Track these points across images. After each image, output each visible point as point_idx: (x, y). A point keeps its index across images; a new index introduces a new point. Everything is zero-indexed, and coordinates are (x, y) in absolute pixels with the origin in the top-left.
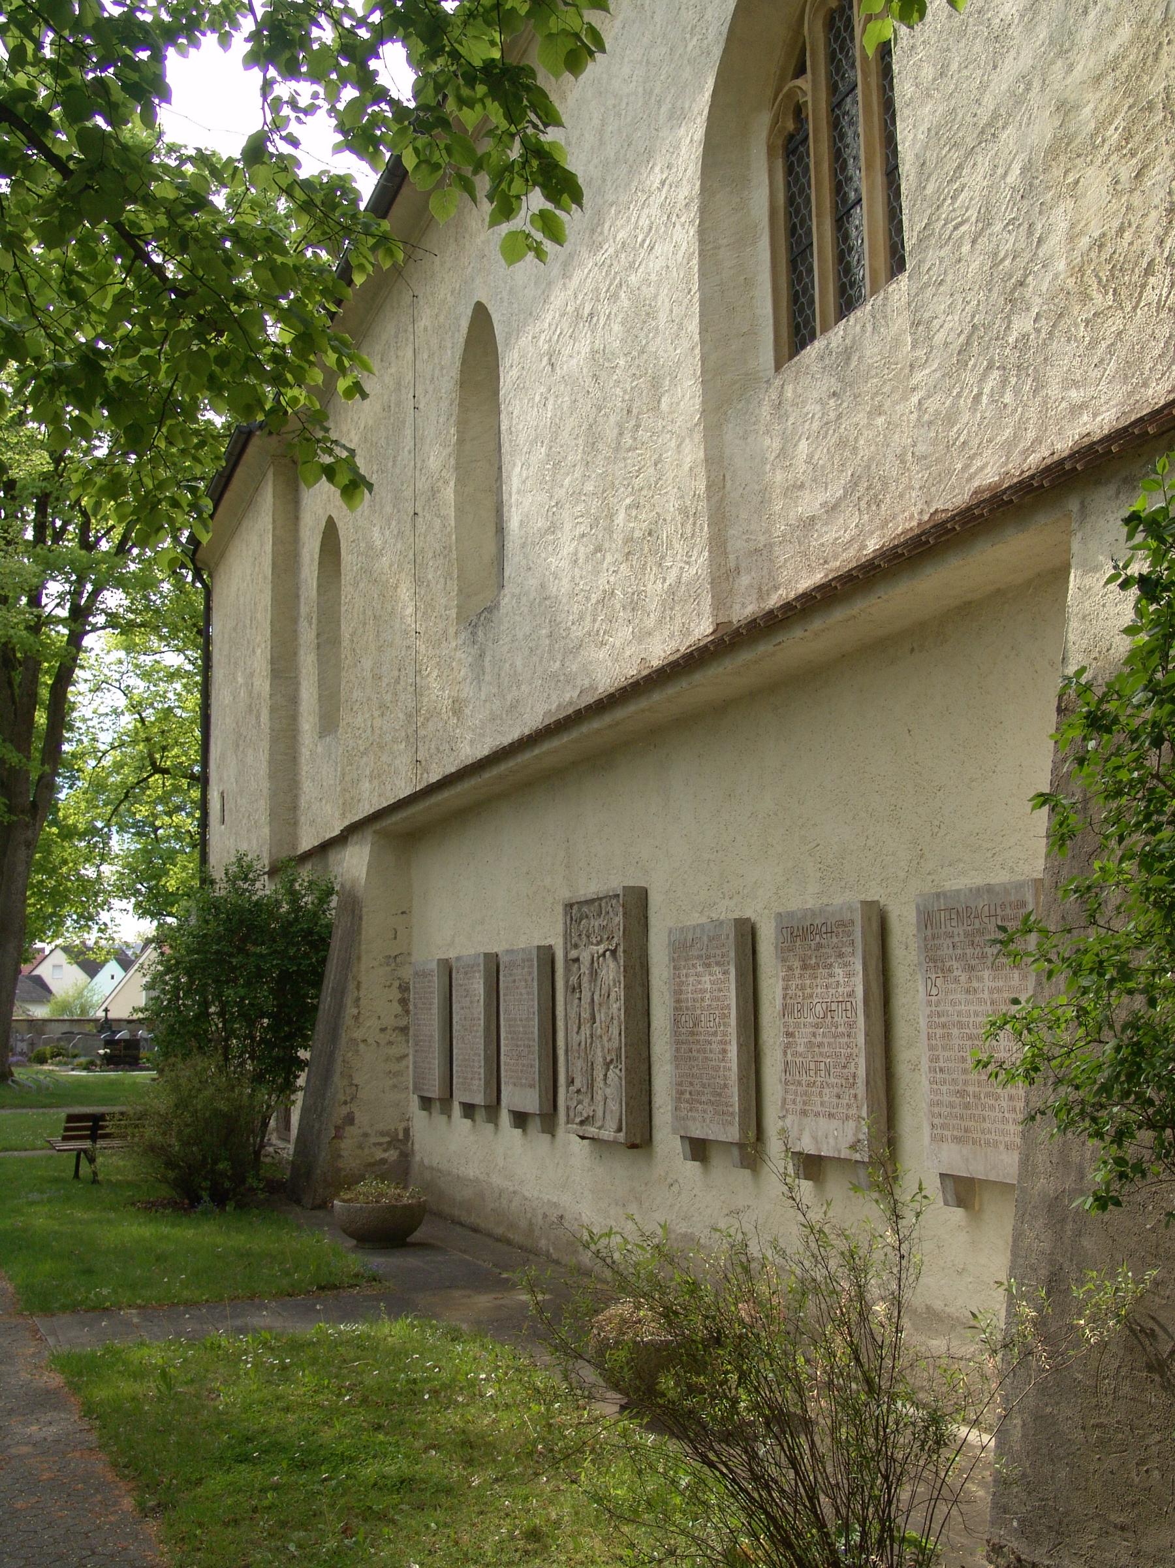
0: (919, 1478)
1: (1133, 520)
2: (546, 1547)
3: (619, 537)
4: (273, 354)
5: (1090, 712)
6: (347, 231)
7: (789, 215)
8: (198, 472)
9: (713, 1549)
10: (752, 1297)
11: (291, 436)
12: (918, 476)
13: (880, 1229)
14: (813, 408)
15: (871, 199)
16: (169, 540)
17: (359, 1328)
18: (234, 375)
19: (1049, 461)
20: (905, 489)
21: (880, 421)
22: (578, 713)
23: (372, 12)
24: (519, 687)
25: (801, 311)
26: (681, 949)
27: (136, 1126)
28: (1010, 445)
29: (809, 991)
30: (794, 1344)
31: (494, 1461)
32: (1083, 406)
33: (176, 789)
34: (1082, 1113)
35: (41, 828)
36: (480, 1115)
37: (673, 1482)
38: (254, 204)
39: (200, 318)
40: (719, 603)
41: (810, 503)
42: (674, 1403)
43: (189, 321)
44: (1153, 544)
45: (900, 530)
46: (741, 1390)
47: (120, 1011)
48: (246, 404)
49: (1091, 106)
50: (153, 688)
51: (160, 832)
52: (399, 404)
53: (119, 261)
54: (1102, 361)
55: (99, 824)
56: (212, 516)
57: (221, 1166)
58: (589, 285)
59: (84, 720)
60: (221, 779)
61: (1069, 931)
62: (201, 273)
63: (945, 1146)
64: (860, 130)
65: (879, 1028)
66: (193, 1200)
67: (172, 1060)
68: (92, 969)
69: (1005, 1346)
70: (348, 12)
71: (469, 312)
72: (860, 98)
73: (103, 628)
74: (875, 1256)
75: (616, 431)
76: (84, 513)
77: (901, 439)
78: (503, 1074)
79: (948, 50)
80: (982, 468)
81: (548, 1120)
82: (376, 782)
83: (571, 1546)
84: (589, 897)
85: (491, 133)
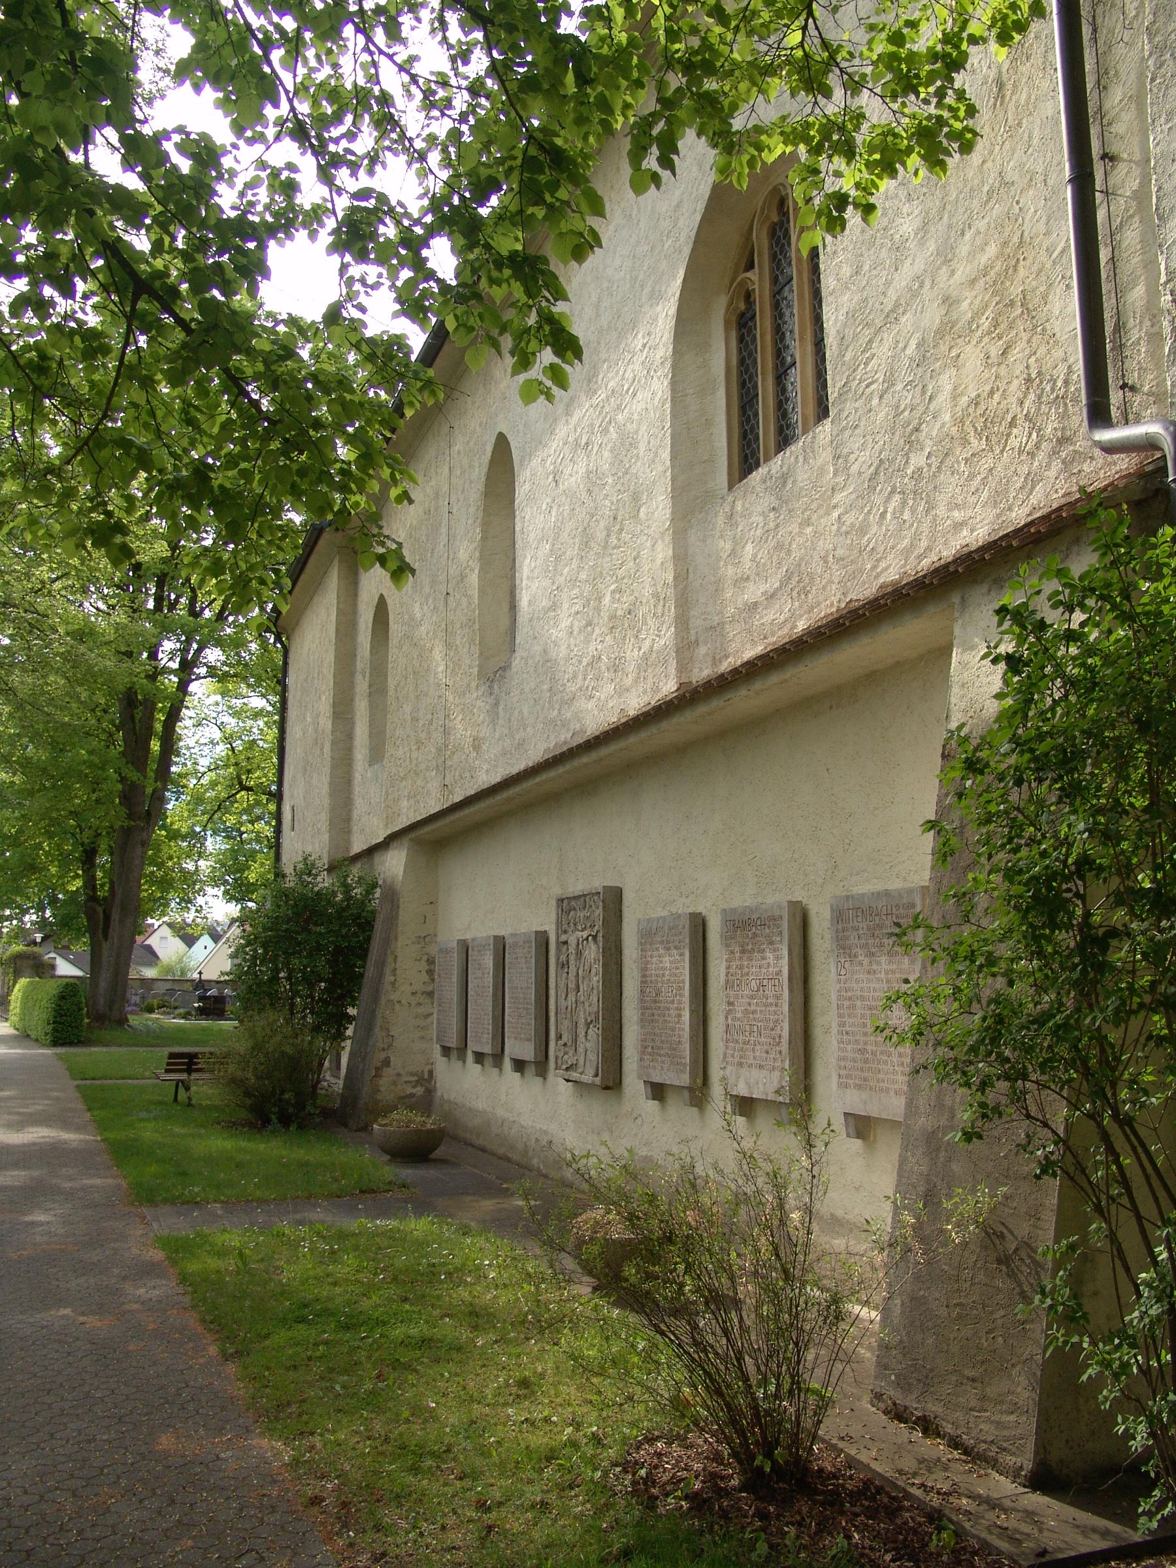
0: (821, 1344)
1: (1002, 611)
2: (533, 1393)
3: (605, 615)
4: (341, 469)
5: (967, 758)
6: (401, 376)
7: (740, 374)
8: (280, 558)
9: (662, 1396)
10: (698, 1207)
11: (352, 532)
12: (837, 573)
13: (797, 1155)
14: (757, 519)
15: (803, 363)
16: (257, 610)
17: (392, 1223)
18: (311, 484)
19: (937, 565)
20: (827, 583)
21: (809, 530)
22: (571, 750)
23: (426, 214)
24: (525, 729)
25: (749, 445)
26: (648, 935)
27: (222, 1063)
28: (907, 552)
29: (746, 970)
30: (729, 1242)
31: (494, 1327)
32: (962, 524)
33: (258, 803)
34: (955, 1068)
35: (154, 832)
36: (488, 1062)
37: (632, 1346)
38: (331, 355)
39: (286, 440)
40: (682, 668)
41: (754, 592)
42: (634, 1286)
43: (277, 443)
44: (1017, 630)
45: (823, 614)
46: (687, 1277)
47: (211, 974)
48: (319, 507)
49: (968, 301)
50: (241, 724)
51: (245, 836)
52: (437, 508)
53: (226, 397)
54: (977, 490)
55: (198, 829)
56: (290, 592)
57: (286, 1096)
58: (586, 422)
59: (189, 748)
60: (292, 796)
61: (949, 927)
62: (288, 407)
63: (848, 1091)
64: (795, 311)
65: (800, 999)
66: (266, 1122)
67: (251, 1012)
68: (190, 941)
69: (891, 1245)
70: (407, 215)
71: (493, 440)
72: (795, 288)
73: (205, 677)
74: (793, 1176)
75: (604, 533)
76: (193, 590)
77: (824, 545)
78: (506, 1030)
79: (862, 255)
80: (886, 569)
81: (541, 1066)
82: (412, 801)
83: (552, 1392)
84: (576, 894)
85: (513, 305)
